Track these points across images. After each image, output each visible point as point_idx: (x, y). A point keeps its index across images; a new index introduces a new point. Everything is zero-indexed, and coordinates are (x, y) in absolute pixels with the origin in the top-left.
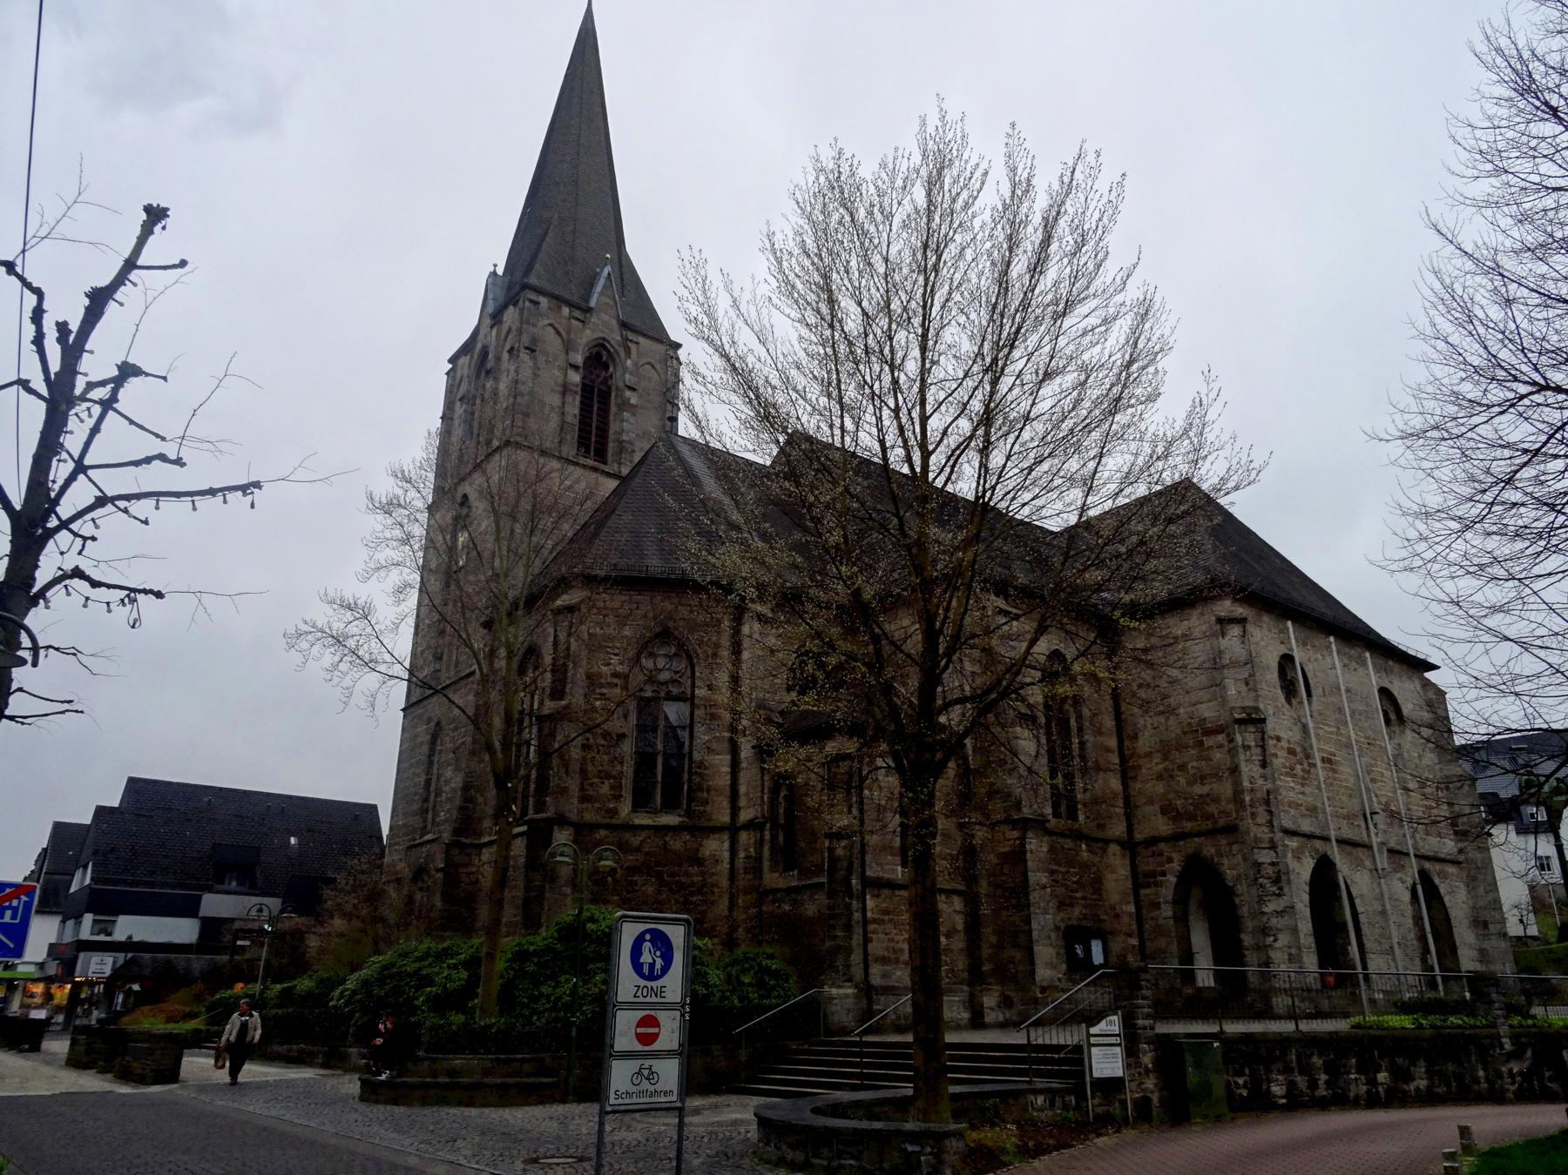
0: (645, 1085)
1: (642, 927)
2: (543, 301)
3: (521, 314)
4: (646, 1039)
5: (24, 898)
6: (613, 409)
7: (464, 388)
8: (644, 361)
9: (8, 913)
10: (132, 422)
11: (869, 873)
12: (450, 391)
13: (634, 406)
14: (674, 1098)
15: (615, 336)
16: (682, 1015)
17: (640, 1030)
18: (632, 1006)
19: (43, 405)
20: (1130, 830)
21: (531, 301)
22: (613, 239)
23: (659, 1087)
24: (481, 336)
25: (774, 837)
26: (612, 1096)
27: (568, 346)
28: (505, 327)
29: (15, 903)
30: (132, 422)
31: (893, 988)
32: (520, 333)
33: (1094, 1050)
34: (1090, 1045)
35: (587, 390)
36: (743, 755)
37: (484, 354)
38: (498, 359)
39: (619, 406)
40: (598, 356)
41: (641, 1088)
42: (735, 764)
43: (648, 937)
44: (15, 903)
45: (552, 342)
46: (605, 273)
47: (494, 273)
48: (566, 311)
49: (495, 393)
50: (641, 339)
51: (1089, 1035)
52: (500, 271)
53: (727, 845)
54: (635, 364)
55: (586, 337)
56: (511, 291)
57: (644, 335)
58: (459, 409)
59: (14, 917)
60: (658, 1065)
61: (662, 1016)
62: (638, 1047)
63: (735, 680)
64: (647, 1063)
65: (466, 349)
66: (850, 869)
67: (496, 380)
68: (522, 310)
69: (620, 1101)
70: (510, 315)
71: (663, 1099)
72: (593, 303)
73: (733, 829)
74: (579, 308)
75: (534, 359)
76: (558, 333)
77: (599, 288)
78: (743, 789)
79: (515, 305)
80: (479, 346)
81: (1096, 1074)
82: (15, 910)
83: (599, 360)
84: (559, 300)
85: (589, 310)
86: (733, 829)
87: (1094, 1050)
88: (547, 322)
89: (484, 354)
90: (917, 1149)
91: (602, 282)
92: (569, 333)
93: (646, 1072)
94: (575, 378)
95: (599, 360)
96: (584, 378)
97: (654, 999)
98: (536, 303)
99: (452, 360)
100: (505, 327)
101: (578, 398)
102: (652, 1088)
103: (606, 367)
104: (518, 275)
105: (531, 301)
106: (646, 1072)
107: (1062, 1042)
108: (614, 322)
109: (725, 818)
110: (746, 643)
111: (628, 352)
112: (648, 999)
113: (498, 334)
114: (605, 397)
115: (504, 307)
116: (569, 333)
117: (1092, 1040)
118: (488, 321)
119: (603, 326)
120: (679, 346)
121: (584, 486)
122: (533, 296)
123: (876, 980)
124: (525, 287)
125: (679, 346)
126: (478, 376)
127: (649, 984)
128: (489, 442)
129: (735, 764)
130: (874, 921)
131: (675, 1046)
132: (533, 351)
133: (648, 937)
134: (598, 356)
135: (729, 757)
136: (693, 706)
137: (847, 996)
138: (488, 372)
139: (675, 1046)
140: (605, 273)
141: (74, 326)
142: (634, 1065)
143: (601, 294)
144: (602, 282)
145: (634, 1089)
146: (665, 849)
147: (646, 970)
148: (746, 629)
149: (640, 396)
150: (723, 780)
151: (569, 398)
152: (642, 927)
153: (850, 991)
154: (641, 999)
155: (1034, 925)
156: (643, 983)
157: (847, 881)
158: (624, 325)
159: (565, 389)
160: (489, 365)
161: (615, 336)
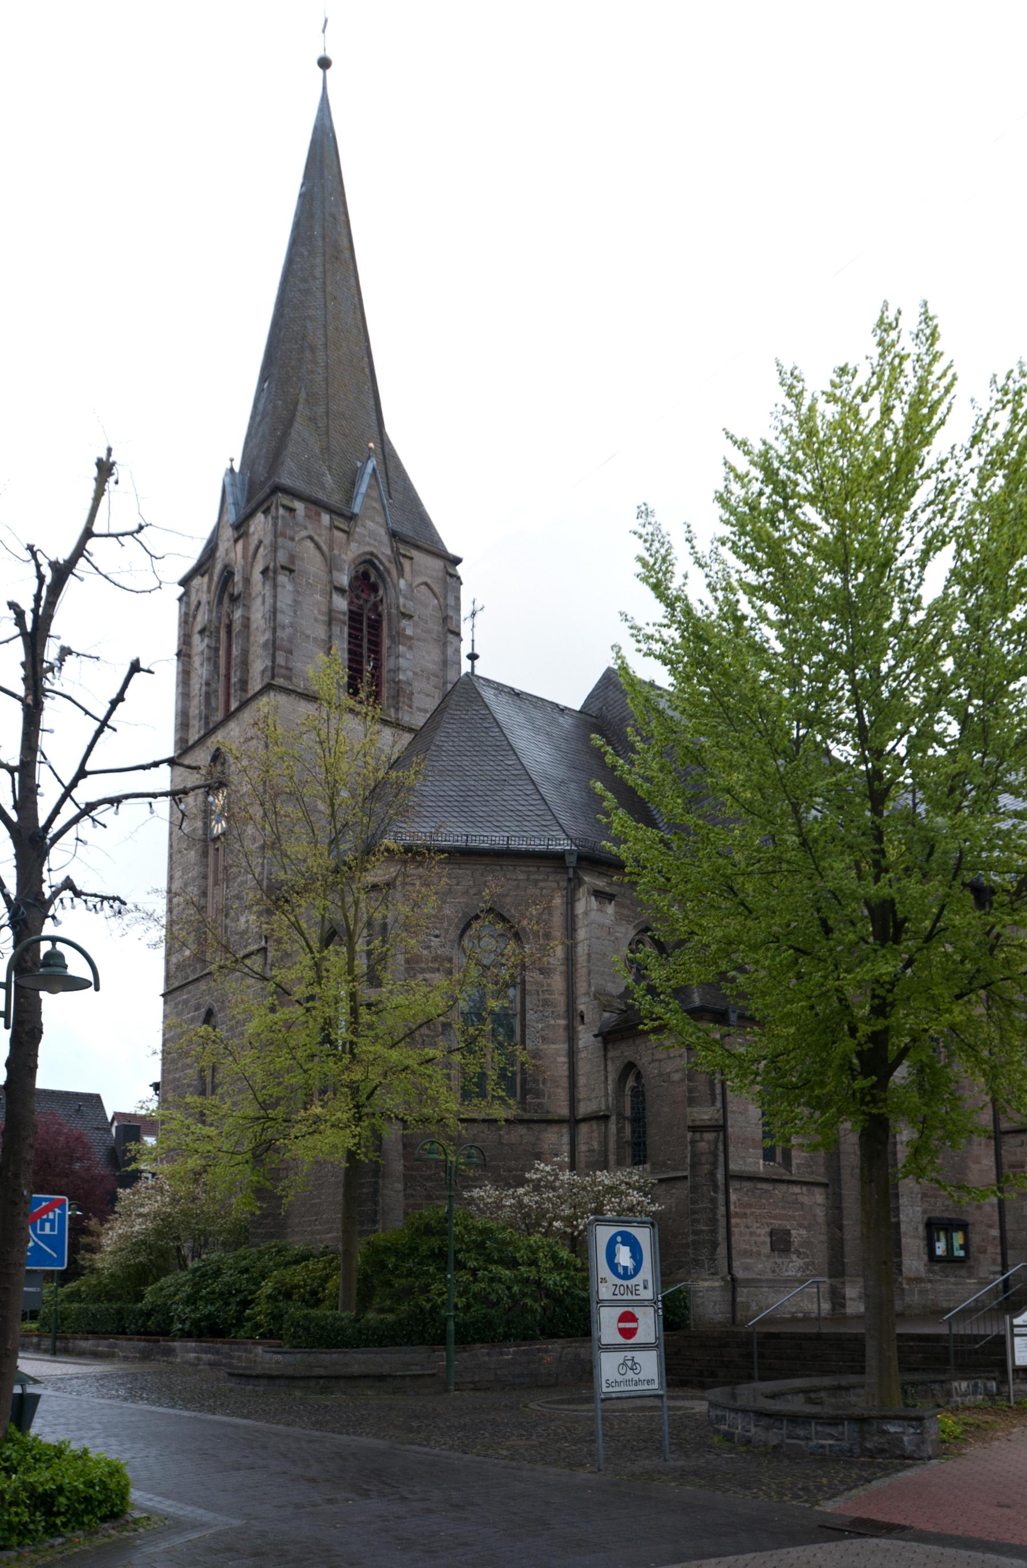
0: (630, 1375)
1: (613, 1230)
2: (299, 506)
3: (275, 525)
4: (628, 1333)
5: (57, 1211)
6: (386, 642)
7: (202, 619)
8: (419, 580)
9: (47, 1225)
10: (87, 713)
11: (732, 1166)
12: (186, 621)
13: (410, 638)
14: (656, 1386)
15: (384, 550)
16: (656, 1311)
17: (622, 1325)
18: (612, 1303)
19: (19, 705)
20: (996, 1121)
21: (284, 507)
22: (374, 424)
23: (642, 1377)
24: (220, 552)
25: (620, 1130)
26: (604, 1385)
27: (331, 565)
28: (254, 541)
29: (51, 1216)
30: (87, 713)
31: (753, 1280)
32: (275, 548)
33: (1017, 1340)
34: (1013, 1335)
35: (355, 618)
36: (581, 1044)
37: (228, 574)
38: (247, 581)
39: (392, 638)
40: (366, 575)
41: (626, 1377)
42: (572, 1054)
43: (619, 1239)
44: (51, 1216)
45: (312, 562)
46: (369, 469)
47: (232, 470)
48: (326, 518)
49: (246, 622)
50: (414, 553)
51: (1013, 1326)
52: (237, 469)
53: (566, 1139)
54: (410, 586)
55: (350, 554)
56: (257, 490)
57: (418, 547)
58: (200, 645)
59: (52, 1229)
60: (640, 1356)
61: (638, 1312)
62: (620, 1340)
63: (570, 960)
64: (629, 1355)
65: (201, 568)
66: (714, 1164)
67: (247, 607)
68: (275, 518)
69: (611, 1389)
70: (260, 524)
71: (646, 1387)
72: (356, 509)
73: (573, 1122)
74: (341, 515)
75: (292, 580)
76: (318, 547)
77: (363, 489)
78: (582, 1081)
79: (266, 512)
80: (218, 567)
81: (1018, 1363)
82: (52, 1222)
83: (367, 580)
84: (316, 504)
85: (351, 518)
86: (573, 1122)
87: (1017, 1340)
88: (304, 533)
89: (228, 574)
90: (899, 1430)
91: (366, 478)
92: (331, 549)
93: (629, 1363)
94: (341, 604)
95: (367, 580)
96: (351, 603)
97: (630, 1297)
98: (291, 510)
99: (185, 582)
100: (254, 541)
101: (346, 629)
102: (636, 1377)
103: (374, 588)
104: (261, 469)
105: (284, 507)
106: (629, 1363)
107: (982, 1332)
108: (382, 532)
109: (564, 1111)
110: (580, 922)
111: (401, 573)
112: (625, 1297)
113: (245, 549)
114: (376, 626)
115: (251, 515)
116: (331, 549)
117: (1016, 1331)
118: (228, 533)
119: (372, 536)
120: (457, 561)
121: (365, 742)
122: (285, 500)
123: (740, 1274)
124: (278, 489)
125: (457, 561)
126: (220, 602)
127: (625, 1283)
128: (244, 683)
129: (572, 1054)
130: (737, 1214)
131: (652, 1339)
132: (291, 571)
133: (619, 1239)
134: (366, 575)
135: (566, 1046)
136: (524, 992)
137: (713, 1289)
138: (234, 599)
139: (652, 1339)
140: (369, 469)
141: (27, 605)
142: (618, 1357)
143: (367, 495)
144: (366, 478)
145: (619, 1378)
146: (500, 1143)
147: (621, 1271)
148: (580, 907)
149: (415, 626)
150: (563, 1071)
151: (336, 630)
152: (613, 1230)
153: (717, 1284)
154: (619, 1297)
155: (902, 1217)
156: (619, 1282)
157: (712, 1174)
158: (394, 535)
159: (331, 620)
160: (238, 588)
161: (384, 550)
